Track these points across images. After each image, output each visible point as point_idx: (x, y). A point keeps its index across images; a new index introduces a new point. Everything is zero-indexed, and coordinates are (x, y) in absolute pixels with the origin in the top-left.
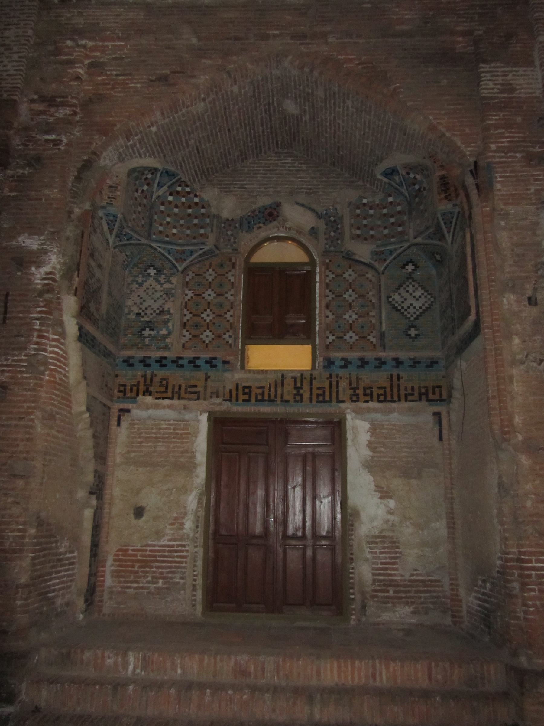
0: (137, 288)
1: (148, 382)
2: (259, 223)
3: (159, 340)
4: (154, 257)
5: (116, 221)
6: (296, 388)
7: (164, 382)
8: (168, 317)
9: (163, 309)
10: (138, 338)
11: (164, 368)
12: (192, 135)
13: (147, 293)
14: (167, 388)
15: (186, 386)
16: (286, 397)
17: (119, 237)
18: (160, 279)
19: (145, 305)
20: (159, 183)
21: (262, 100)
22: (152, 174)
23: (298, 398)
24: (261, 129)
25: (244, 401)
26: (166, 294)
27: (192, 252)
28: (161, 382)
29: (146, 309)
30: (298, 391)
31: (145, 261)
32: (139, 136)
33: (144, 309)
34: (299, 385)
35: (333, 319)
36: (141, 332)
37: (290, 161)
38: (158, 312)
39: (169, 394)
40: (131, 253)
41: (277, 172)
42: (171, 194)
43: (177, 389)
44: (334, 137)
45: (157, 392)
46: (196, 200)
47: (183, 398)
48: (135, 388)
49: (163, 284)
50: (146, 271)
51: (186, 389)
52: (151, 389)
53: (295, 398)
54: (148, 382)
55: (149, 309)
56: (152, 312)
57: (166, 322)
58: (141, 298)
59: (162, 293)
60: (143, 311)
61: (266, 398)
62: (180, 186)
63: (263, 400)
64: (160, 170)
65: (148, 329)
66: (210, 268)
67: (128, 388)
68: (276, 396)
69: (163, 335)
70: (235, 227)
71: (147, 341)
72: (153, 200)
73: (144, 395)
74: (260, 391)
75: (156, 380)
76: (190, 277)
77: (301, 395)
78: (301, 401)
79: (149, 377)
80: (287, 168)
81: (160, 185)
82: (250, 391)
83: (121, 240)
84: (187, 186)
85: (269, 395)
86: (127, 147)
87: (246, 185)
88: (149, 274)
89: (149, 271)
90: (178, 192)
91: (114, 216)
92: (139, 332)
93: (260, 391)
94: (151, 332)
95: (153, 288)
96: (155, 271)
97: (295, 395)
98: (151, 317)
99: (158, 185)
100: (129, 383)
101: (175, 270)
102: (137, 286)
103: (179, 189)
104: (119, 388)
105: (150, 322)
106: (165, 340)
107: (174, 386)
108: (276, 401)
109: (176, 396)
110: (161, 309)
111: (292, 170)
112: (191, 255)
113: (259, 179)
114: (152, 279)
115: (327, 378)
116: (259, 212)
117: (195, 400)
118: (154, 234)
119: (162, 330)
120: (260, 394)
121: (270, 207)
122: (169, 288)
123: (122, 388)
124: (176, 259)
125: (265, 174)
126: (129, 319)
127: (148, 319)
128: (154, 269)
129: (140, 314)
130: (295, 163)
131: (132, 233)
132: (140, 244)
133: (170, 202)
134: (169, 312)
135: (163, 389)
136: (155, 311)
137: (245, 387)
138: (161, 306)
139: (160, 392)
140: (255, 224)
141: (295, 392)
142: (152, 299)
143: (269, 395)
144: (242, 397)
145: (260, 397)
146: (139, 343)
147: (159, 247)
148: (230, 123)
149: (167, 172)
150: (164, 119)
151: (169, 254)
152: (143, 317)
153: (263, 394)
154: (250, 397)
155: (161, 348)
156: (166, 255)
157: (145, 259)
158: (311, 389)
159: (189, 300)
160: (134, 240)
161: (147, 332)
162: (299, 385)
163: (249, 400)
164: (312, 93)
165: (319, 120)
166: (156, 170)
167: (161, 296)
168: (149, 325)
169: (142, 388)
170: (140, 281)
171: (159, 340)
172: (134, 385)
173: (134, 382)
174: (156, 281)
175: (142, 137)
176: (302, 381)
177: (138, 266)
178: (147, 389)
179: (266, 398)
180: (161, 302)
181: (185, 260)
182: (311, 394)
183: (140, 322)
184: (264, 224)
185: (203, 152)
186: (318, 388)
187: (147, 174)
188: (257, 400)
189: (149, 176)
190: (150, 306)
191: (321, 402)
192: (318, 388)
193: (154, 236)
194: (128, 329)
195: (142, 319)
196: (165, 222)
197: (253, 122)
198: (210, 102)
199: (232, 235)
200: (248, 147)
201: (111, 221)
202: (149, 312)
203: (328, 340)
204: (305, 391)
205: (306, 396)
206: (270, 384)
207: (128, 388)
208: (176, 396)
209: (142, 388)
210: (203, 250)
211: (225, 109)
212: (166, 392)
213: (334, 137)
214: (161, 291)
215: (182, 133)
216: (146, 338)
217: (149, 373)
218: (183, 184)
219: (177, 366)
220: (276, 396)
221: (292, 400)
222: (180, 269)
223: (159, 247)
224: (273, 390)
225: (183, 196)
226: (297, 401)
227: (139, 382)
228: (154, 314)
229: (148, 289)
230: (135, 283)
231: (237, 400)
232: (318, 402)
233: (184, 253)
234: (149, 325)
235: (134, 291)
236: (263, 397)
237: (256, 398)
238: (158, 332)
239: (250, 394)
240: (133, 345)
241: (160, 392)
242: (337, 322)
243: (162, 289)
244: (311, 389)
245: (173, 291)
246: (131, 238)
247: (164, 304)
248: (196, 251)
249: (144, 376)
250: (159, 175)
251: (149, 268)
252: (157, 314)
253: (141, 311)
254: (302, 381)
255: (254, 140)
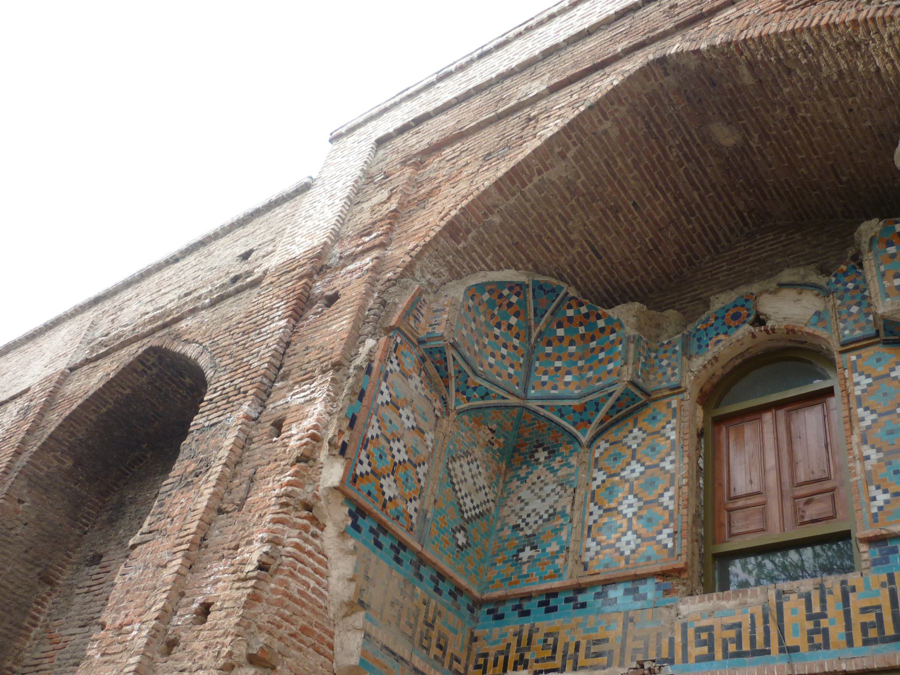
0: (518, 487)
1: (524, 644)
2: (718, 334)
3: (545, 564)
4: (540, 427)
5: (446, 359)
6: (809, 617)
7: (551, 640)
8: (562, 521)
9: (555, 510)
10: (512, 566)
11: (552, 614)
12: (570, 224)
13: (533, 491)
14: (554, 651)
15: (588, 642)
16: (789, 642)
17: (464, 393)
18: (553, 464)
19: (528, 509)
20: (535, 309)
21: (669, 138)
22: (518, 294)
23: (818, 639)
24: (695, 194)
25: (700, 659)
26: (562, 485)
27: (597, 404)
28: (545, 641)
29: (529, 516)
30: (817, 624)
31: (527, 439)
32: (474, 233)
33: (524, 516)
34: (816, 609)
35: (879, 460)
36: (517, 555)
37: (772, 237)
38: (546, 516)
39: (558, 663)
40: (498, 424)
41: (751, 259)
42: (560, 325)
43: (571, 651)
44: (815, 153)
45: (537, 661)
46: (601, 323)
47: (583, 667)
48: (501, 658)
49: (558, 470)
50: (532, 456)
51: (588, 649)
52: (528, 656)
53: (811, 640)
54: (524, 644)
55: (533, 514)
56: (537, 518)
57: (557, 531)
58: (522, 501)
59: (554, 486)
60: (524, 521)
61: (746, 647)
62: (570, 307)
63: (739, 654)
64: (528, 286)
65: (528, 548)
66: (634, 427)
67: (491, 659)
68: (767, 641)
69: (552, 553)
70: (675, 352)
71: (525, 569)
72: (533, 340)
73: (515, 669)
74: (732, 634)
75: (538, 637)
76: (601, 450)
77: (825, 632)
78: (826, 645)
79: (525, 634)
80: (767, 248)
81: (538, 315)
82: (711, 636)
83: (468, 399)
84: (581, 304)
85: (753, 640)
86: (458, 252)
87: (701, 293)
88: (537, 460)
89: (537, 455)
90: (570, 319)
91: (440, 352)
92: (513, 556)
93: (732, 634)
94: (533, 553)
95: (542, 481)
96: (546, 454)
97: (810, 632)
98: (535, 527)
99: (535, 315)
100: (492, 650)
101: (577, 444)
102: (519, 483)
103: (570, 313)
104: (476, 661)
105: (534, 535)
106: (553, 562)
107: (567, 645)
108: (768, 652)
109: (569, 664)
110: (551, 511)
111: (777, 248)
112: (598, 410)
113: (721, 279)
114: (541, 467)
115: (883, 585)
116: (716, 318)
117: (604, 668)
118: (533, 388)
119: (550, 545)
120: (733, 642)
121: (735, 306)
122: (568, 475)
123: (481, 661)
124: (574, 424)
125: (730, 269)
126: (500, 538)
127: (529, 532)
128: (544, 450)
129: (519, 525)
130: (781, 237)
131: (486, 384)
132: (507, 407)
133: (561, 339)
134: (563, 514)
135: (549, 653)
136: (541, 517)
137: (699, 630)
138: (551, 507)
139: (543, 660)
140: (711, 339)
141: (810, 625)
142: (540, 497)
143: (753, 640)
144: (695, 651)
145: (732, 648)
146: (512, 574)
147: (543, 407)
148: (630, 192)
149: (541, 287)
150: (507, 200)
151: (562, 416)
152: (522, 530)
153: (738, 640)
154: (711, 649)
155: (546, 578)
156: (557, 418)
157: (526, 435)
158: (847, 614)
159: (598, 487)
160: (494, 398)
161: (524, 556)
162: (816, 609)
163: (710, 657)
164: (735, 86)
165: (774, 132)
166: (520, 285)
167: (553, 490)
168: (532, 542)
169: (513, 656)
170: (523, 475)
171: (545, 564)
172: (501, 652)
173: (502, 646)
174: (548, 469)
175: (480, 233)
176: (823, 601)
177: (519, 450)
178: (522, 656)
179: (746, 647)
180: (550, 501)
181: (590, 422)
182: (848, 626)
183: (518, 538)
184: (726, 333)
185: (605, 252)
186: (864, 610)
187: (509, 296)
188: (726, 655)
189: (514, 299)
190: (534, 510)
191: (874, 641)
192: (864, 610)
193: (533, 392)
194: (498, 555)
195: (521, 534)
196: (552, 368)
197: (673, 181)
198: (575, 158)
199: (668, 365)
200: (687, 232)
201: (438, 362)
202: (530, 520)
203: (874, 503)
204: (832, 622)
205: (837, 631)
206: (752, 617)
207: (491, 659)
208: (569, 664)
209: (513, 656)
210: (615, 396)
211: (608, 165)
212: (552, 658)
213: (815, 153)
214: (554, 482)
215: (550, 222)
216: (524, 563)
217: (527, 627)
218: (574, 303)
219: (575, 608)
220: (767, 641)
221: (804, 646)
222: (584, 440)
223: (543, 407)
224: (760, 629)
225: (581, 324)
226: (818, 647)
227: (509, 645)
228: (540, 522)
229: (533, 484)
230: (515, 480)
231: (685, 659)
232: (866, 642)
233: (585, 410)
234: (532, 542)
235: (513, 492)
236: (739, 644)
237: (725, 649)
238: (544, 550)
239: (710, 643)
240: (502, 581)
241: (543, 660)
242: (890, 463)
243: (555, 479)
244: (847, 614)
245: (573, 478)
246: (487, 394)
247: (556, 502)
248: (604, 400)
249: (518, 634)
250: (530, 295)
251: (537, 451)
252: (544, 521)
253: (520, 521)
254: (823, 601)
255: (693, 219)
